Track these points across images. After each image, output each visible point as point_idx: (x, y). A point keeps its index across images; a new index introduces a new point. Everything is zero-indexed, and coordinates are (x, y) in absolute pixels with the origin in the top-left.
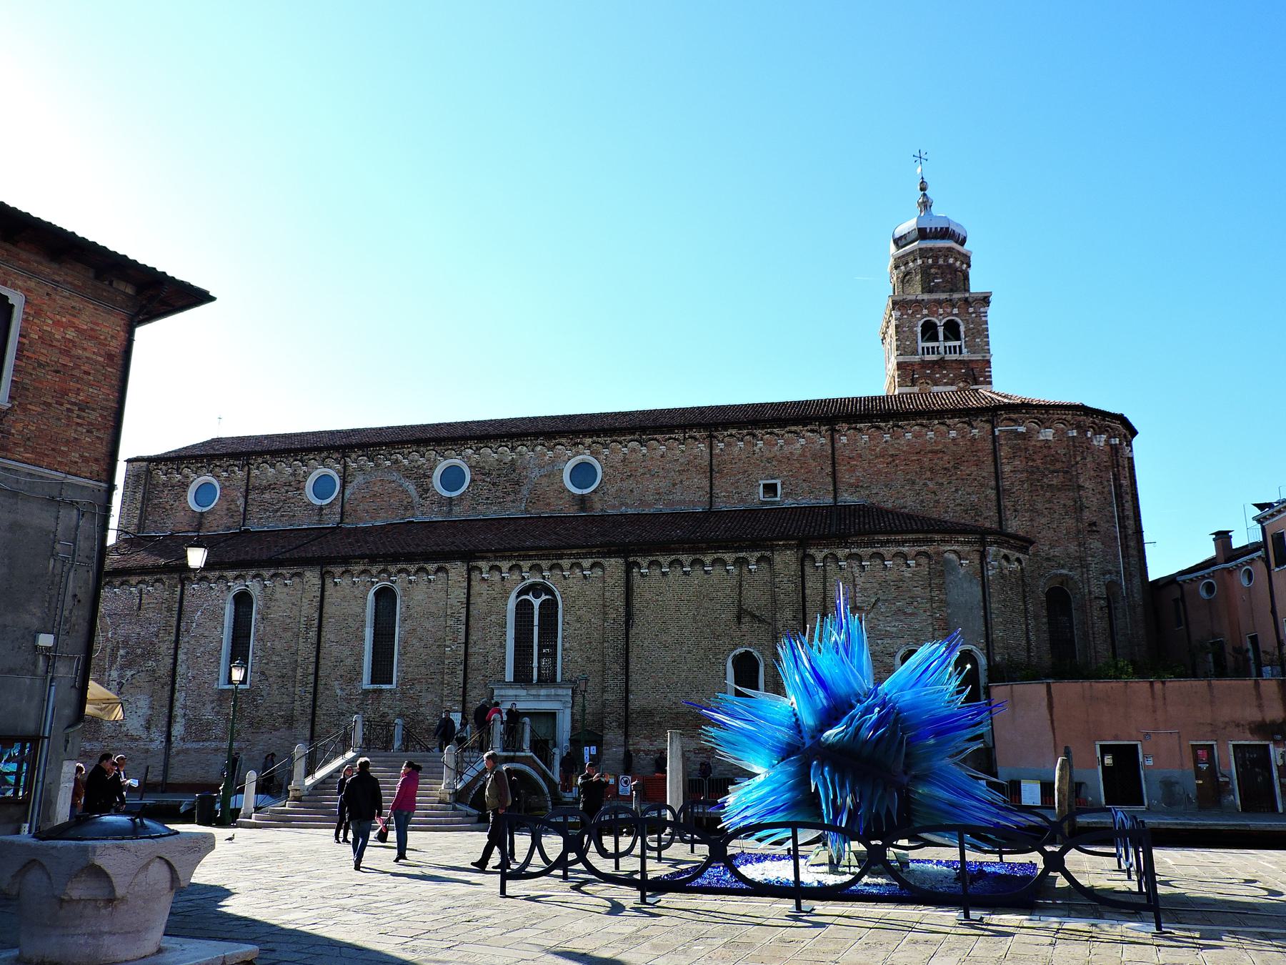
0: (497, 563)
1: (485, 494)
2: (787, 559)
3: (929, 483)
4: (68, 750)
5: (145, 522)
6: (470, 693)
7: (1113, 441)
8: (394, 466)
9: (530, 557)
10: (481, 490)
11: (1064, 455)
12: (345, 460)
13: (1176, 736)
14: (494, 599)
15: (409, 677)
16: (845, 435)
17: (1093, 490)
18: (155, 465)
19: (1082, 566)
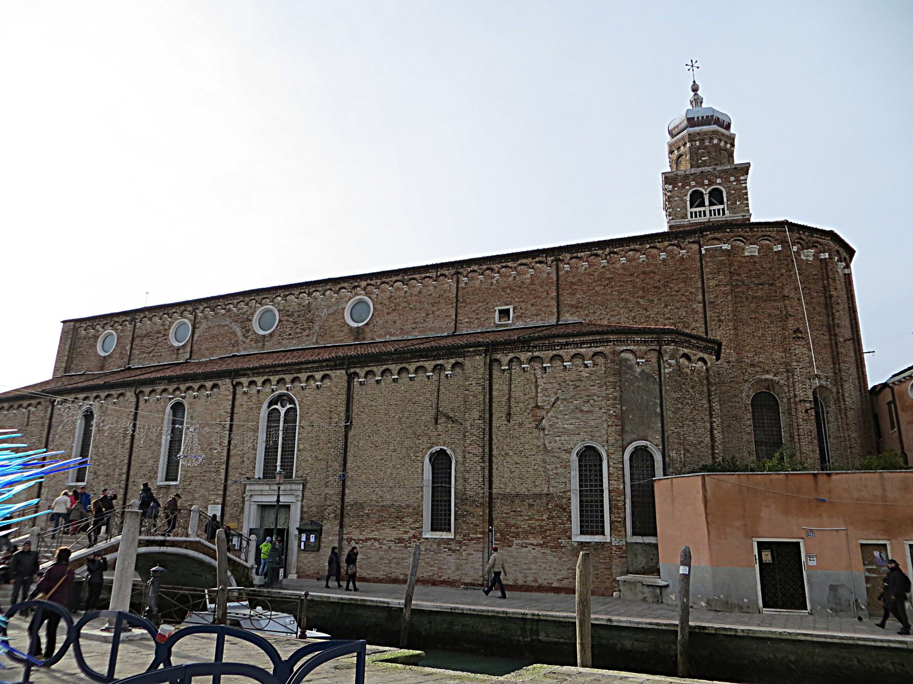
0: (254, 379)
1: (288, 331)
3: (641, 300)
7: (822, 256)
8: (228, 314)
11: (770, 268)
13: (843, 534)
14: (251, 409)
15: (189, 475)
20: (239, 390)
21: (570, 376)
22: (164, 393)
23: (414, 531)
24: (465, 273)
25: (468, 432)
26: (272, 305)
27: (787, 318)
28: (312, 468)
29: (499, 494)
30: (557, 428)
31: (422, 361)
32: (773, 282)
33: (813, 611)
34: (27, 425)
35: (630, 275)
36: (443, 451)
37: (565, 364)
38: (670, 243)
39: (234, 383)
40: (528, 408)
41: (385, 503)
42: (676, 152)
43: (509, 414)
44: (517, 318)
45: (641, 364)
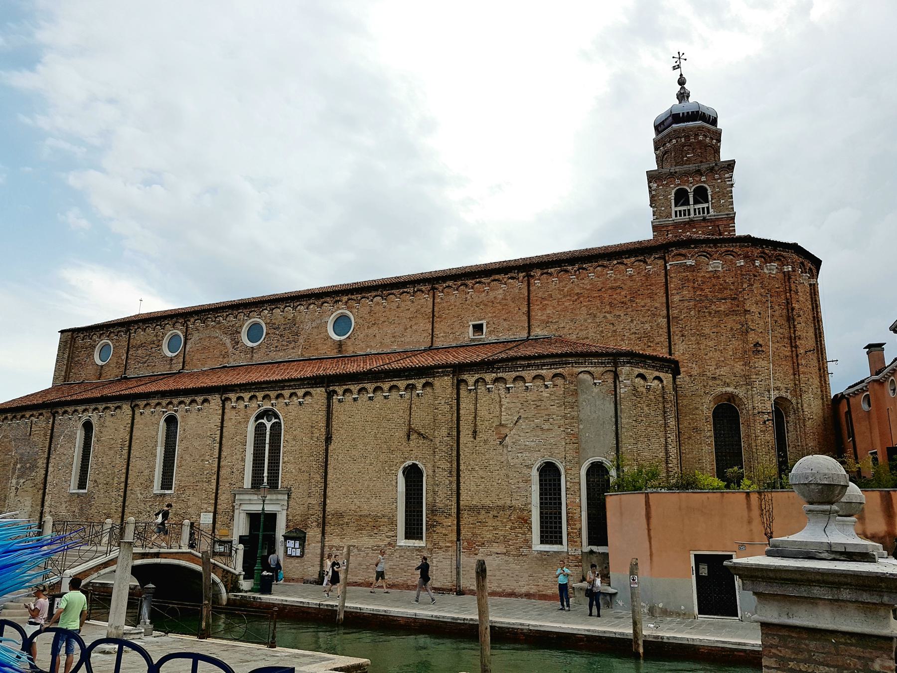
0: (242, 395)
2: (444, 384)
3: (608, 315)
5: (69, 374)
6: (220, 498)
8: (218, 326)
10: (273, 340)
12: (187, 323)
14: (240, 422)
15: (182, 484)
17: (760, 313)
18: (77, 334)
19: (747, 384)
20: (228, 405)
21: (531, 396)
22: (158, 406)
23: (389, 539)
24: (441, 289)
26: (260, 318)
29: (466, 506)
33: (743, 618)
34: (30, 434)
35: (598, 290)
36: (414, 466)
37: (527, 385)
38: (637, 258)
39: (223, 398)
41: (362, 513)
43: (475, 432)
44: (490, 332)
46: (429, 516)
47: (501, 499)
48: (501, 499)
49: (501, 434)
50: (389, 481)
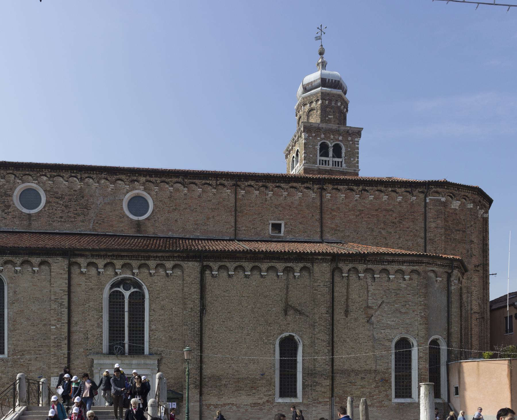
0: (94, 261)
1: (59, 213)
3: (382, 231)
4: (449, 197)
9: (122, 257)
10: (56, 210)
11: (464, 220)
14: (92, 289)
15: (19, 348)
16: (330, 193)
20: (75, 270)
25: (317, 323)
27: (471, 256)
28: (167, 346)
30: (382, 324)
31: (274, 262)
32: (465, 230)
35: (376, 210)
40: (362, 308)
41: (240, 376)
42: (309, 105)
45: (438, 281)
46: (305, 378)
47: (368, 364)
48: (368, 364)
49: (369, 314)
50: (267, 349)
